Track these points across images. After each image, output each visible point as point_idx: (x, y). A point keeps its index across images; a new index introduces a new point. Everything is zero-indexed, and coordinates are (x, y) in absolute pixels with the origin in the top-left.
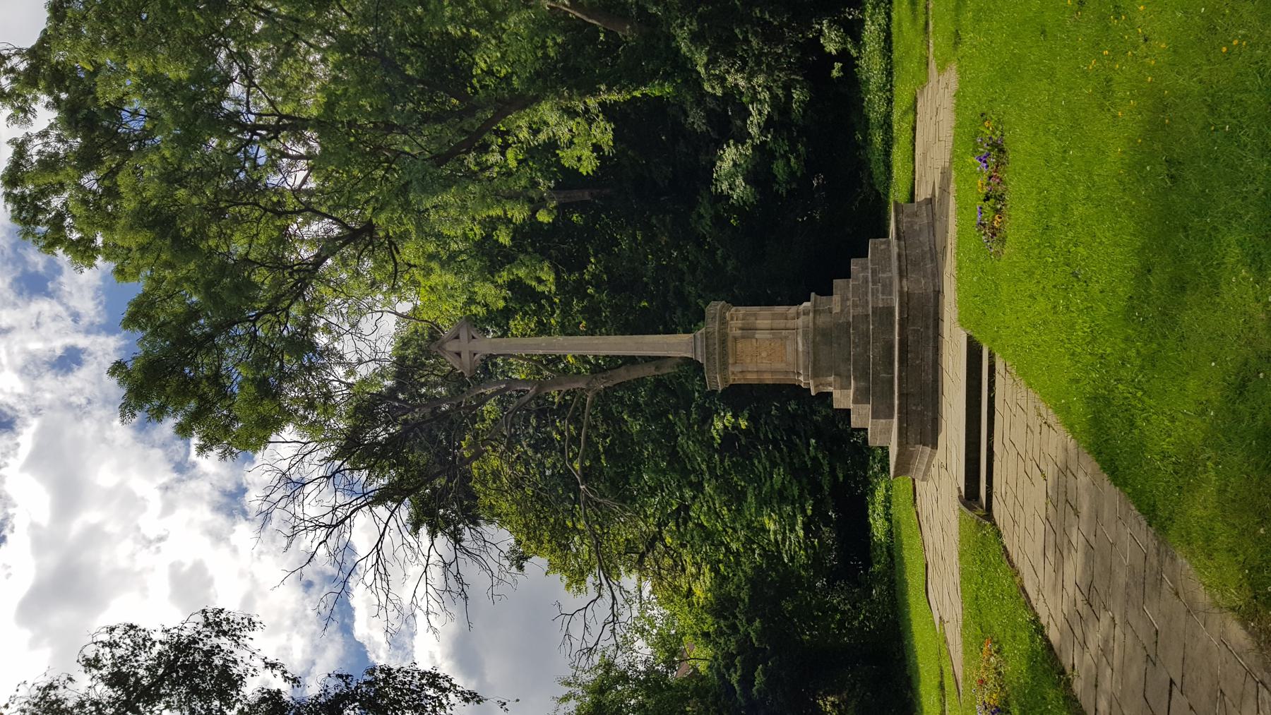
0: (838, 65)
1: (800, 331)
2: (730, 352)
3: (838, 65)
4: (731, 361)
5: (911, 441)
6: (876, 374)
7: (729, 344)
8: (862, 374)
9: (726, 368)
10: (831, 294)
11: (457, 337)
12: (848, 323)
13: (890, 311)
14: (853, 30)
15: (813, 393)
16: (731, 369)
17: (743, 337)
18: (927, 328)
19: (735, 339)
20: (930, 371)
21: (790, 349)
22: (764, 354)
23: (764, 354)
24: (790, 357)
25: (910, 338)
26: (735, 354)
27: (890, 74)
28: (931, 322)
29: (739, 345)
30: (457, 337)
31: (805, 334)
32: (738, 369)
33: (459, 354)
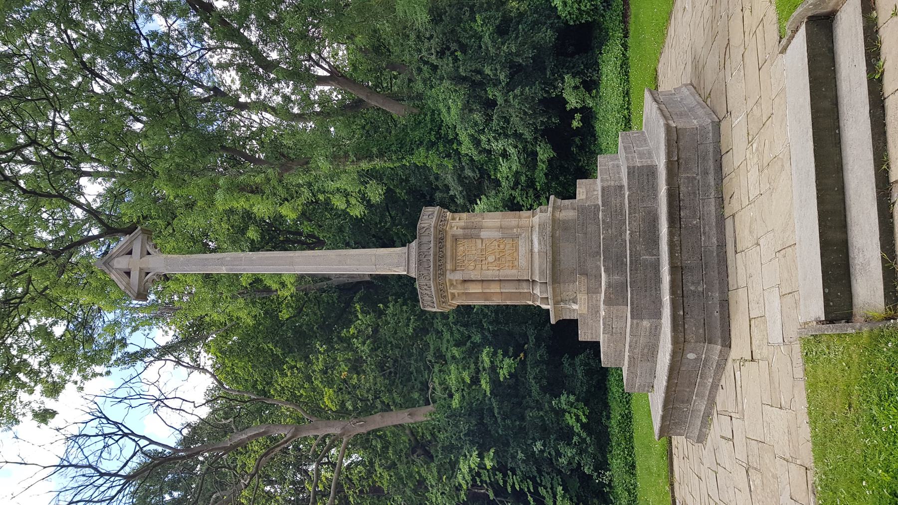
0: (578, 116)
2: (449, 254)
3: (578, 116)
4: (449, 266)
5: (691, 337)
6: (635, 262)
7: (449, 245)
8: (615, 264)
9: (443, 274)
11: (130, 253)
14: (591, 85)
16: (449, 276)
17: (465, 237)
18: (706, 173)
19: (456, 239)
21: (523, 249)
22: (491, 259)
23: (491, 259)
24: (523, 262)
26: (454, 257)
27: (627, 94)
28: (711, 164)
30: (130, 253)
31: (541, 233)
33: (128, 273)
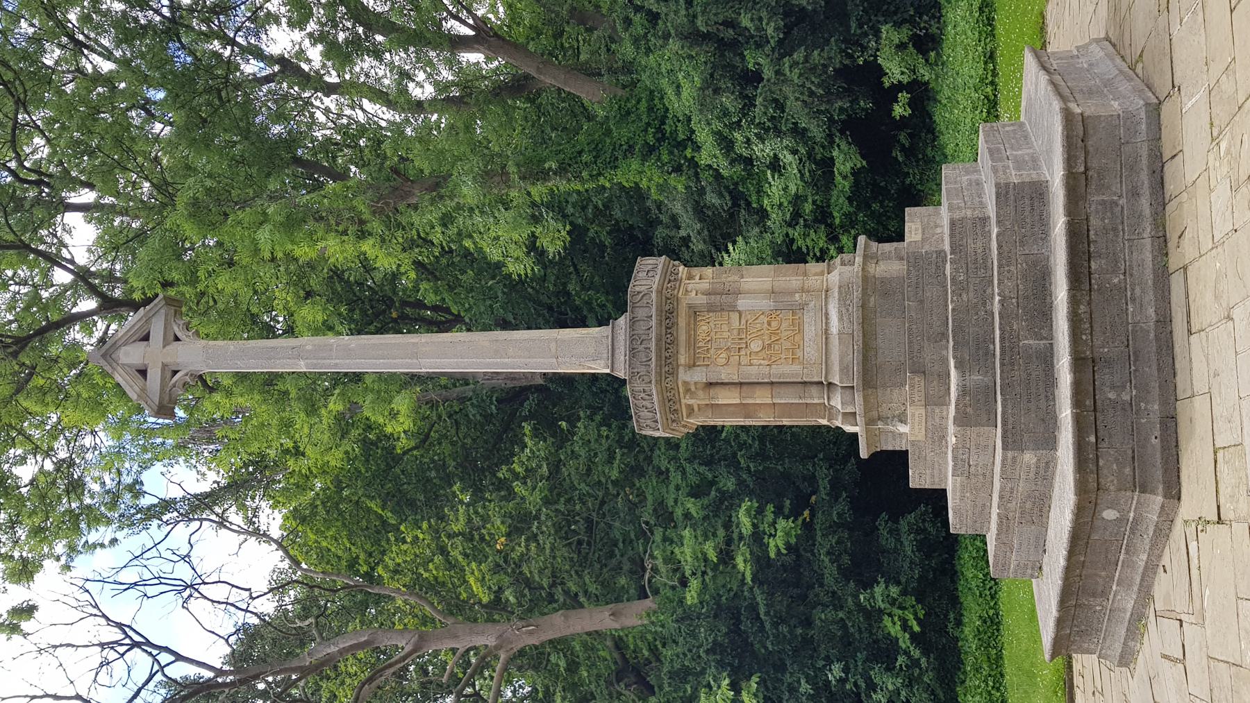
1: (835, 293)
2: (682, 338)
4: (682, 359)
5: (1110, 481)
7: (682, 322)
8: (975, 354)
9: (673, 373)
10: (904, 455)
11: (146, 338)
12: (941, 254)
13: (1038, 192)
14: (927, 43)
15: (864, 454)
16: (683, 376)
17: (711, 308)
18: (1135, 194)
19: (694, 312)
20: (1150, 296)
21: (811, 330)
22: (755, 346)
23: (755, 346)
24: (811, 350)
25: (1095, 222)
26: (692, 343)
29: (703, 328)
30: (146, 338)
31: (843, 300)
32: (699, 376)
33: (143, 373)
